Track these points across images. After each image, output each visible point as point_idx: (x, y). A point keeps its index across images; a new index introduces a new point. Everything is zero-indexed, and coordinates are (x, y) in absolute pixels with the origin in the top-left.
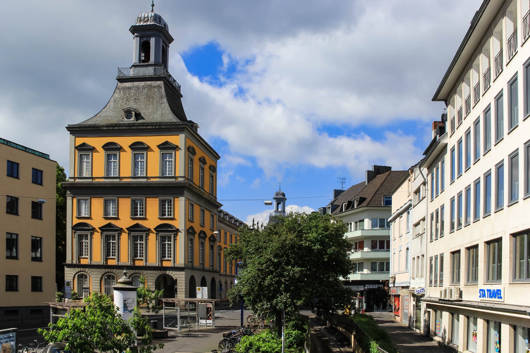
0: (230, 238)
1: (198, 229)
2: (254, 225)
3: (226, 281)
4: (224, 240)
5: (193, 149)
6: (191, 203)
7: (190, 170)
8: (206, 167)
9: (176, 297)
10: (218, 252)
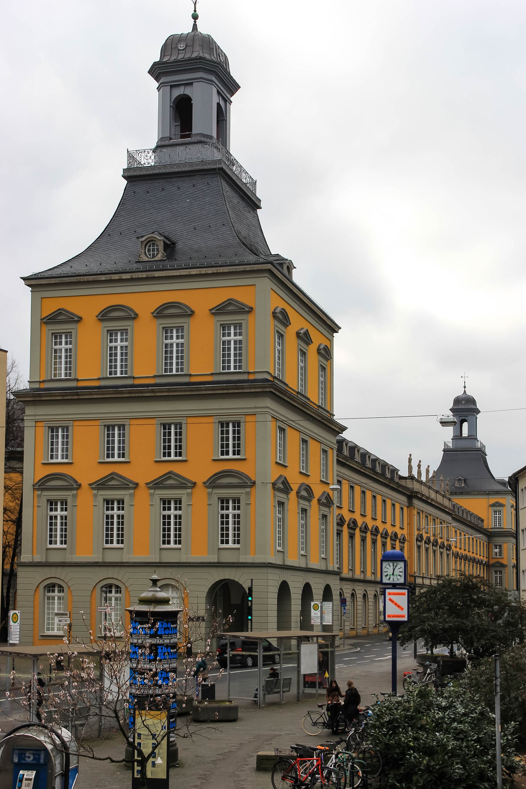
0: (372, 503)
1: (295, 482)
2: (410, 468)
3: (365, 592)
4: (350, 503)
5: (284, 312)
6: (281, 425)
7: (302, 374)
8: (312, 350)
9: (249, 630)
10: (337, 530)
